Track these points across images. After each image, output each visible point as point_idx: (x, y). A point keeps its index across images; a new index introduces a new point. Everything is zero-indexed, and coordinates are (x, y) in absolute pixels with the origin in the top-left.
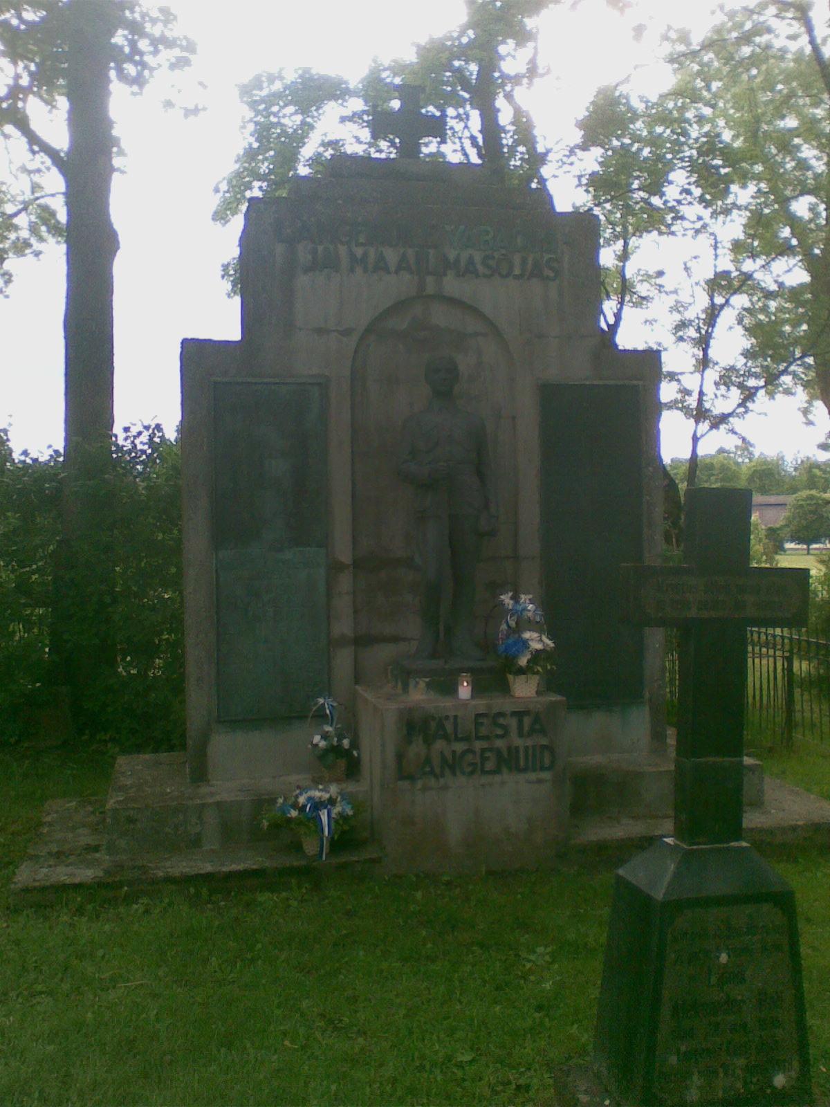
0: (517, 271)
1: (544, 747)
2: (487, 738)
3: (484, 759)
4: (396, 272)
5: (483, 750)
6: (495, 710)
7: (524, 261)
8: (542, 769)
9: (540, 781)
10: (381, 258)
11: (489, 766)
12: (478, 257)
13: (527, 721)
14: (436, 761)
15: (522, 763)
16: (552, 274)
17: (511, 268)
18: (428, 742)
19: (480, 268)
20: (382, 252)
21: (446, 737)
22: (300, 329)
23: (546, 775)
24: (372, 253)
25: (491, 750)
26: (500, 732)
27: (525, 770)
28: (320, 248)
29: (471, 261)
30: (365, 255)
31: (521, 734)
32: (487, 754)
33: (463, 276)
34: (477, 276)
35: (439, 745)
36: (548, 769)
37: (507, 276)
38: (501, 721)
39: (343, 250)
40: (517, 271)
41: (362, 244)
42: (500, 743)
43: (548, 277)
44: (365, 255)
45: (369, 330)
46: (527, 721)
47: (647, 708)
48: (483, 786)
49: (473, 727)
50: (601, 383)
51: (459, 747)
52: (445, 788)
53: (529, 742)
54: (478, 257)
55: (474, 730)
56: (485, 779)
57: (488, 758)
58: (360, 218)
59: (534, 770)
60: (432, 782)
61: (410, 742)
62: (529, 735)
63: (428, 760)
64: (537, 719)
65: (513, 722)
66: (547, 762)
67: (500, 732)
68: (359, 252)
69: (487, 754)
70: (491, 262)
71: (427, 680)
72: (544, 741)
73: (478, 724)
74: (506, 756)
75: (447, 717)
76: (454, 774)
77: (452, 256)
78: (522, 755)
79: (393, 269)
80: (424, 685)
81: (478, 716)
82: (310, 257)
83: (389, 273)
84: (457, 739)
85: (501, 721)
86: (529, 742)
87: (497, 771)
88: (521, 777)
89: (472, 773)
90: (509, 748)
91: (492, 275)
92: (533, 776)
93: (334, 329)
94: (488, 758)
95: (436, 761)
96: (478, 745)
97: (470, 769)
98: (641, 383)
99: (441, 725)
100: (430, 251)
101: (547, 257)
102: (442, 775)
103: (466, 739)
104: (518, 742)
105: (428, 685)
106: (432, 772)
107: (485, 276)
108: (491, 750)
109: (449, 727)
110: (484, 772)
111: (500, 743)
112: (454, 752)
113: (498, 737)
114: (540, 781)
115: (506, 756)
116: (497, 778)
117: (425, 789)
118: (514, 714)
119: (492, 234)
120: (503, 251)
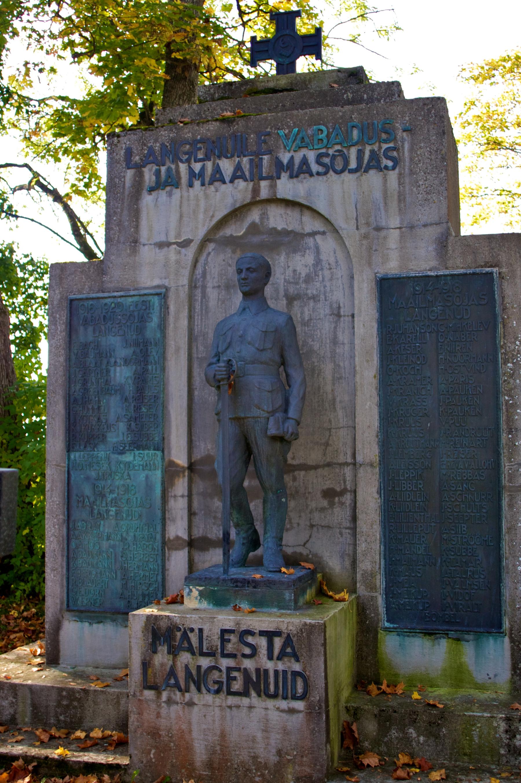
0: (353, 165)
1: (295, 674)
2: (232, 656)
3: (230, 679)
4: (232, 181)
5: (229, 669)
6: (244, 628)
7: (360, 154)
8: (295, 698)
9: (292, 711)
10: (217, 170)
11: (237, 686)
12: (311, 156)
13: (278, 642)
14: (181, 675)
15: (272, 688)
16: (390, 164)
17: (346, 162)
18: (173, 652)
19: (315, 168)
20: (218, 164)
21: (190, 650)
22: (144, 245)
23: (300, 705)
24: (209, 165)
25: (238, 669)
26: (247, 651)
27: (275, 696)
28: (163, 169)
29: (305, 161)
30: (203, 168)
31: (270, 657)
32: (235, 674)
33: (297, 176)
34: (311, 175)
35: (185, 658)
36: (302, 698)
37: (342, 171)
38: (250, 639)
39: (183, 167)
40: (353, 165)
41: (200, 160)
42: (248, 664)
43: (386, 167)
44: (203, 168)
45: (206, 240)
46: (278, 642)
47: (507, 639)
48: (230, 707)
49: (219, 644)
50: (447, 272)
51: (205, 662)
52: (191, 704)
53: (280, 666)
54: (311, 156)
55: (219, 647)
56: (232, 700)
57: (235, 678)
58: (199, 137)
59: (285, 698)
60: (178, 696)
61: (155, 652)
62: (279, 658)
63: (172, 673)
64: (288, 641)
65: (263, 642)
66: (300, 690)
67: (247, 651)
68: (197, 167)
69: (235, 674)
70: (327, 160)
71: (201, 588)
72: (297, 667)
73: (224, 641)
74: (255, 679)
75: (192, 630)
76: (199, 690)
77: (285, 158)
78: (272, 680)
79: (227, 179)
80: (197, 593)
81: (224, 632)
82: (154, 178)
83: (224, 182)
84: (203, 654)
85: (250, 639)
86: (280, 666)
87: (245, 693)
88: (271, 703)
89: (218, 692)
90: (258, 670)
91: (326, 173)
92: (284, 704)
93: (174, 241)
94: (235, 678)
95: (181, 675)
96: (225, 663)
97: (216, 687)
98: (495, 270)
99: (185, 636)
100: (264, 157)
101: (385, 146)
102: (187, 690)
103: (211, 654)
104: (270, 665)
105: (202, 594)
106: (177, 686)
107: (318, 174)
108: (238, 669)
109: (194, 638)
110: (230, 693)
111: (248, 664)
112: (199, 667)
113: (244, 656)
114: (292, 711)
115: (255, 679)
116: (245, 701)
117: (170, 702)
118: (262, 633)
119: (326, 132)
120: (338, 147)
